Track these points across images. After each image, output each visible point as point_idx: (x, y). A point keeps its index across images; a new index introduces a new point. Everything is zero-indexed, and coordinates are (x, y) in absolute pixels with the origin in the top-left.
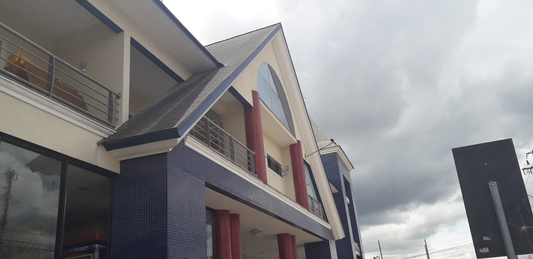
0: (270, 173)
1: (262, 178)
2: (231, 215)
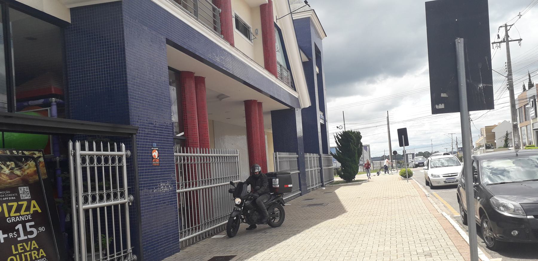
0: (237, 35)
1: (229, 39)
2: (196, 77)
